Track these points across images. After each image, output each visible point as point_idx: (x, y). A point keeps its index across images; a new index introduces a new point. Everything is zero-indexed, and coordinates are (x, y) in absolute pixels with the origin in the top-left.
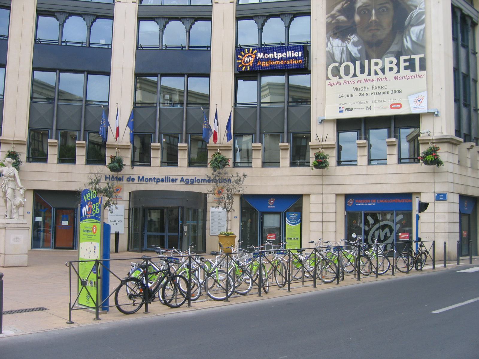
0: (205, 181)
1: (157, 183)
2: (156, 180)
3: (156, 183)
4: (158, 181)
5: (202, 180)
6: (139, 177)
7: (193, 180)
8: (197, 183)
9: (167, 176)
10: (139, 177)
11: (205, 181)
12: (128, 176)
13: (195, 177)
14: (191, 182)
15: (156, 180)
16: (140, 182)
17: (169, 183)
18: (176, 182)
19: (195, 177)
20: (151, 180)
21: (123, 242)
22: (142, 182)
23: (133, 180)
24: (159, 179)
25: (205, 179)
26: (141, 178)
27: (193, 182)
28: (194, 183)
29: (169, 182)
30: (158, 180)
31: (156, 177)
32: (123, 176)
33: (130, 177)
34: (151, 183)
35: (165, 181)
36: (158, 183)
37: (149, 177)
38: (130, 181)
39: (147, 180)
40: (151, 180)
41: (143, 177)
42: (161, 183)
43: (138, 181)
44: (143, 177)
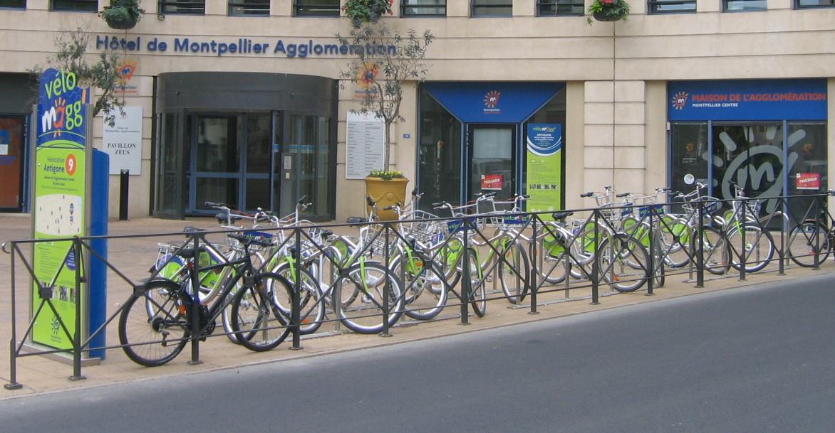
0: (334, 50)
1: (219, 55)
2: (216, 48)
3: (216, 54)
4: (223, 49)
5: (327, 47)
6: (177, 41)
7: (305, 46)
8: (314, 55)
9: (243, 39)
10: (177, 41)
11: (334, 50)
12: (151, 39)
13: (311, 41)
14: (302, 52)
15: (216, 48)
16: (178, 53)
17: (247, 55)
18: (264, 52)
19: (311, 41)
20: (205, 48)
21: (140, 194)
22: (184, 53)
23: (163, 47)
24: (224, 45)
25: (335, 46)
26: (181, 43)
27: (305, 53)
28: (309, 55)
29: (249, 52)
30: (223, 48)
31: (218, 41)
32: (139, 39)
33: (156, 39)
34: (205, 53)
35: (238, 50)
36: (222, 55)
37: (200, 41)
38: (155, 49)
39: (196, 48)
40: (205, 48)
41: (186, 41)
42: (228, 54)
43: (176, 50)
44: (186, 41)
